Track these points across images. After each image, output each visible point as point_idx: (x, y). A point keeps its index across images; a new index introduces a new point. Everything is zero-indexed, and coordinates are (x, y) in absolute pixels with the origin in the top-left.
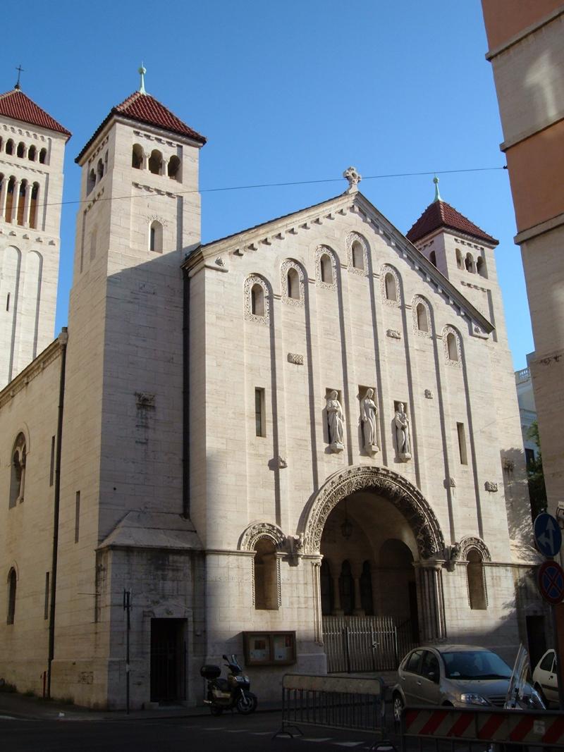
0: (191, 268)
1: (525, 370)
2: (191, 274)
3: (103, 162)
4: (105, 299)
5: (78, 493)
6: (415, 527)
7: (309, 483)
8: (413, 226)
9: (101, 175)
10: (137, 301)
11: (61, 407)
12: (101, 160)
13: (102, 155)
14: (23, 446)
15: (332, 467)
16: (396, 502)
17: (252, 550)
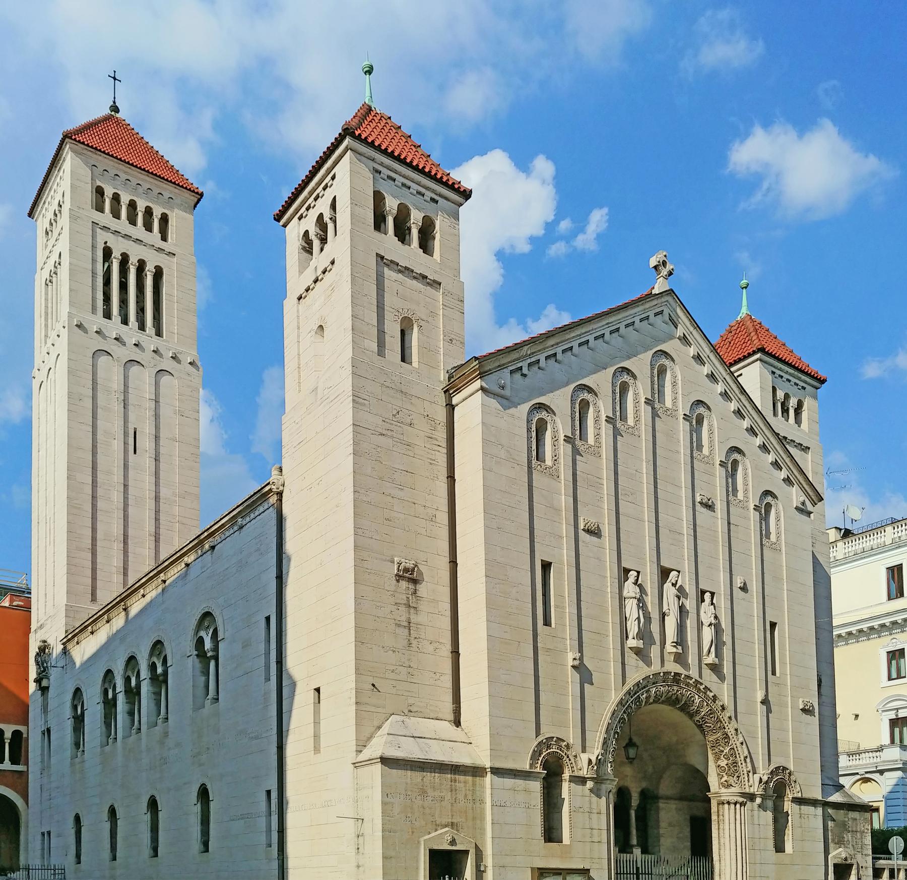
0: (458, 390)
1: (838, 563)
2: (455, 401)
3: (326, 219)
4: (351, 429)
5: (318, 690)
6: (717, 750)
7: (442, 674)
8: (9, 761)
9: (324, 240)
10: (389, 433)
11: (451, 478)
12: (321, 216)
13: (323, 207)
14: (136, 670)
15: (637, 672)
16: (697, 718)
17: (539, 769)
